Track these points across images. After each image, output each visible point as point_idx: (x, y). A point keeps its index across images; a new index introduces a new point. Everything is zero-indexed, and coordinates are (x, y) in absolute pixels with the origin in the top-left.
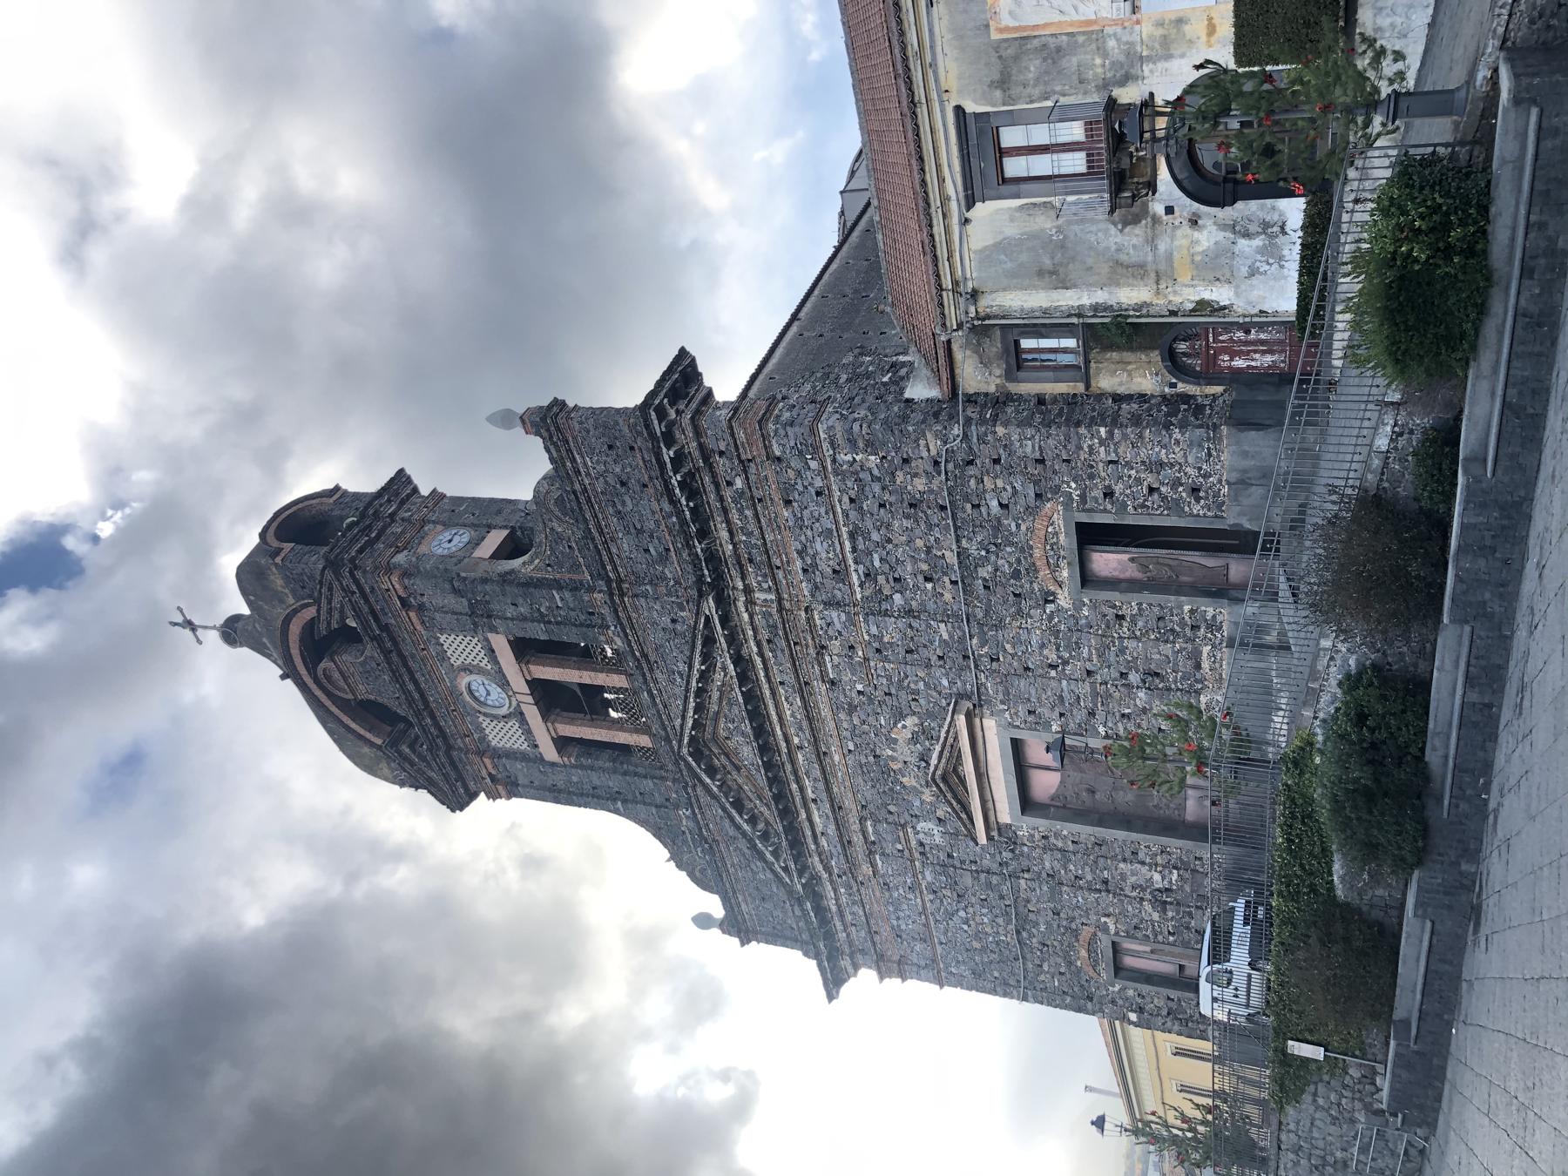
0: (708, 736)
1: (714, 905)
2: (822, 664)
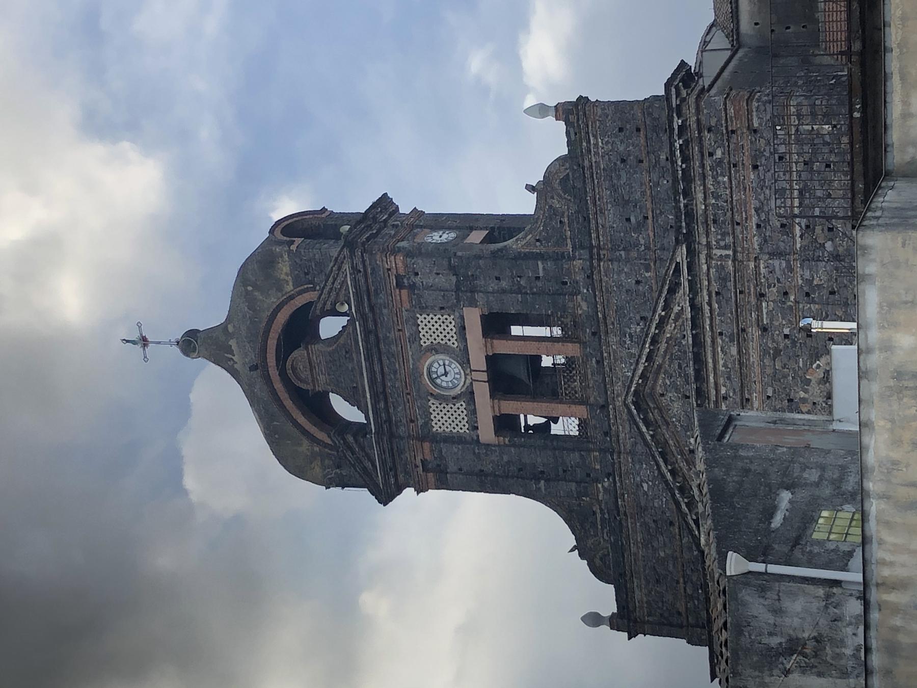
0: (647, 390)
2: (759, 308)
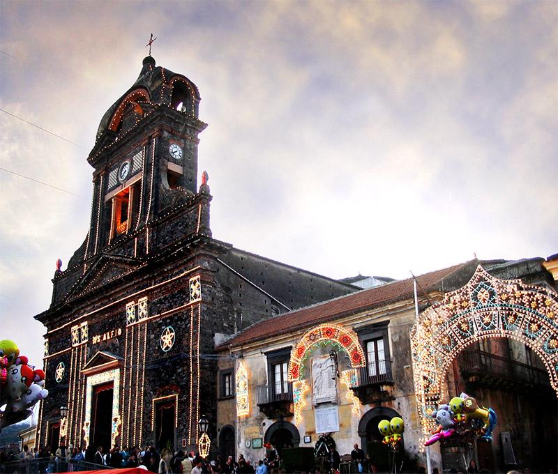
1: (64, 268)
